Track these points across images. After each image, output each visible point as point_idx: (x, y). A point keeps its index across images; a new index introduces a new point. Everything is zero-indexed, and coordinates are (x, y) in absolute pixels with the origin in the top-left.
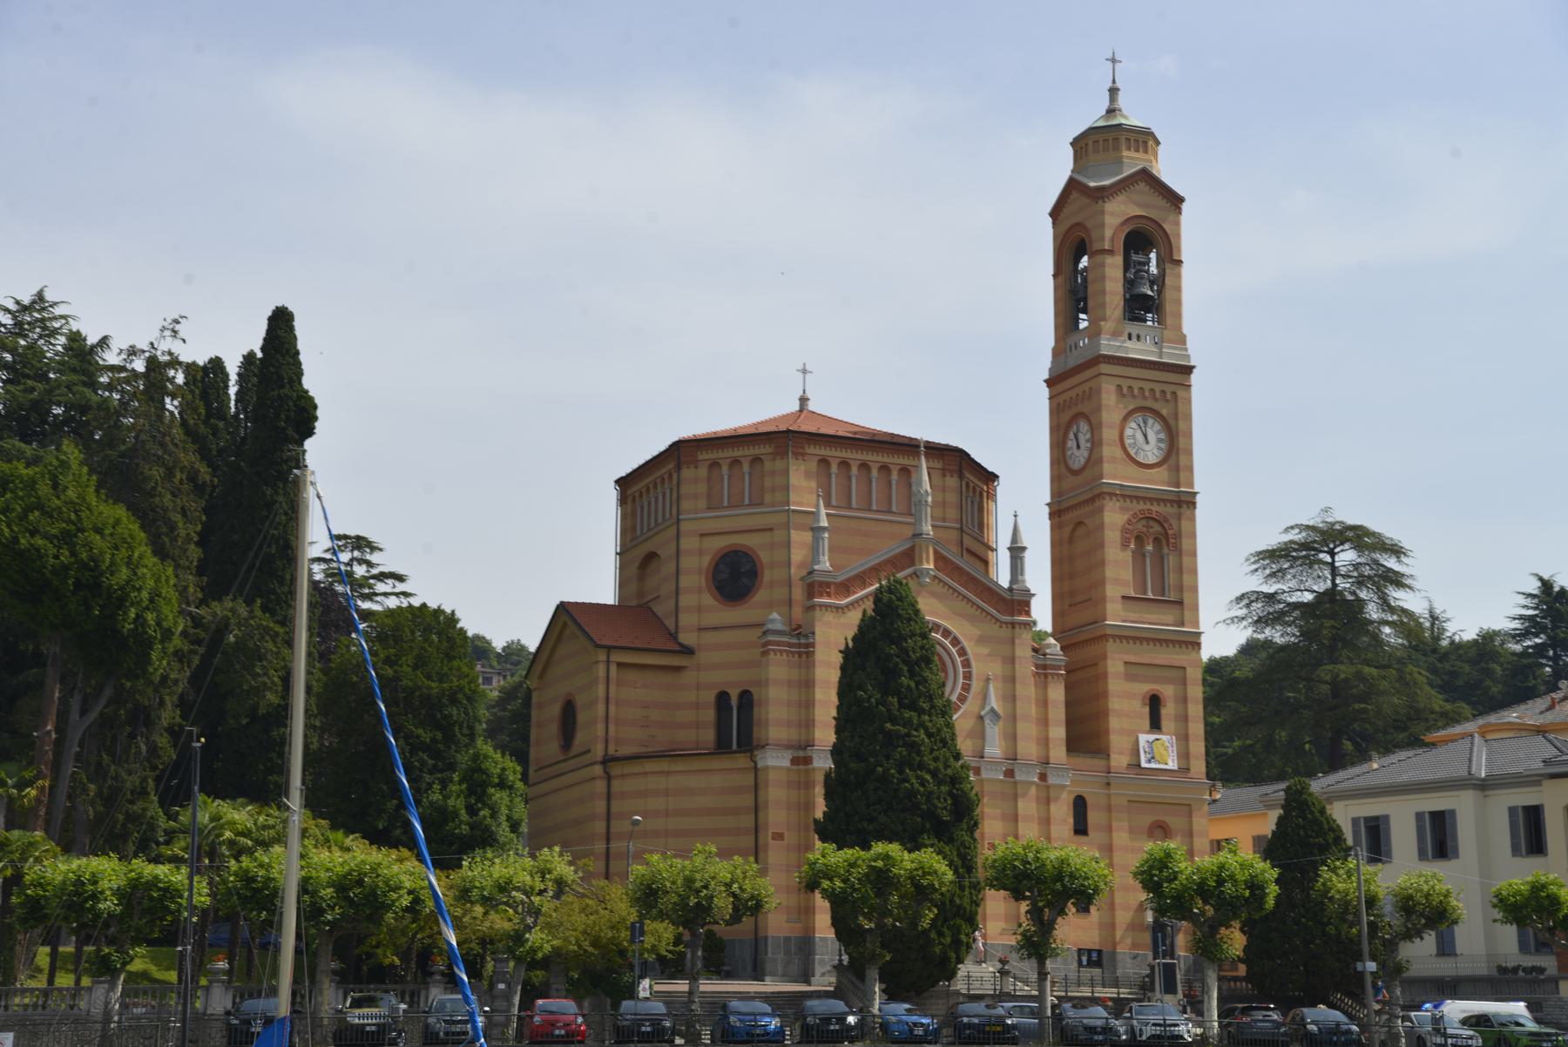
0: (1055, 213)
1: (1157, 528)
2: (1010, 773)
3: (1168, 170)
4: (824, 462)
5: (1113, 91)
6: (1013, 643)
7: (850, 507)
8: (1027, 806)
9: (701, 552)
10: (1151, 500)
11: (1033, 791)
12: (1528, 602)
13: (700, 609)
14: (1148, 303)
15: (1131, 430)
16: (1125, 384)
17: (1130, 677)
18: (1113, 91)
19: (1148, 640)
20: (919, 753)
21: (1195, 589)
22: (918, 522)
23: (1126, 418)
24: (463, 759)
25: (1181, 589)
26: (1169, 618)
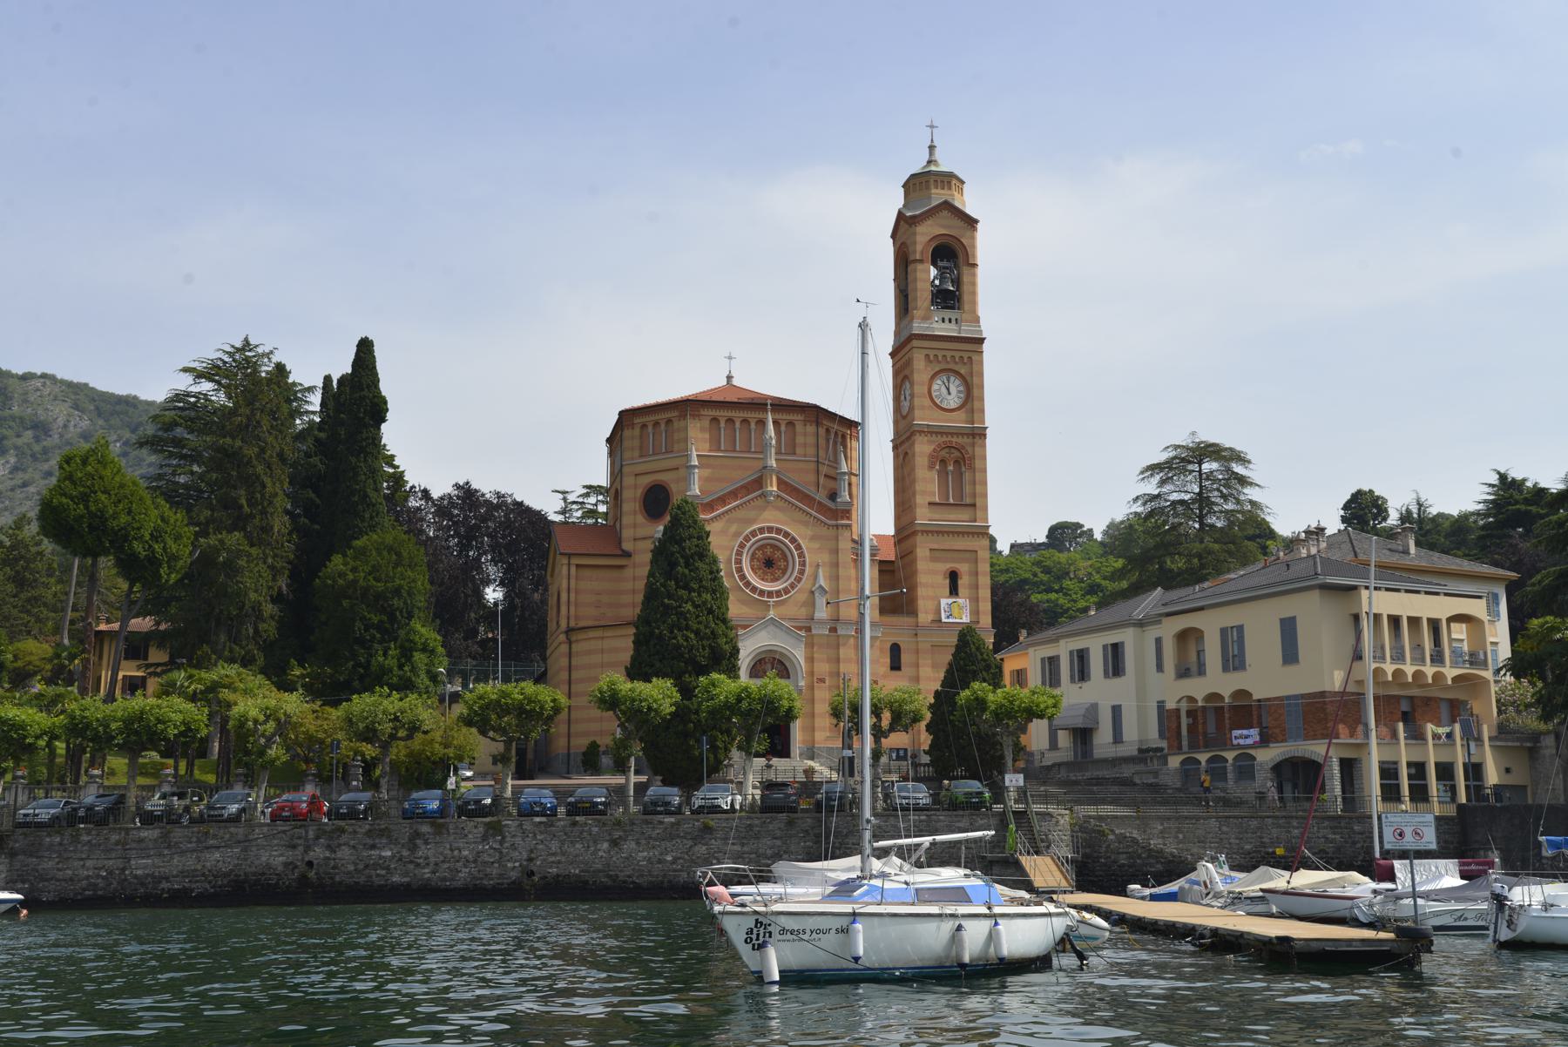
0: (894, 236)
1: (957, 454)
2: (833, 630)
3: (970, 203)
4: (715, 420)
5: (932, 148)
6: (837, 539)
7: (719, 450)
8: (847, 652)
9: (636, 486)
10: (952, 434)
11: (852, 641)
12: (1490, 490)
13: (635, 526)
14: (951, 298)
15: (938, 385)
16: (932, 353)
17: (934, 559)
18: (932, 148)
19: (948, 533)
20: (686, 619)
21: (985, 495)
22: (765, 459)
23: (933, 378)
24: (402, 633)
25: (974, 495)
26: (966, 517)
